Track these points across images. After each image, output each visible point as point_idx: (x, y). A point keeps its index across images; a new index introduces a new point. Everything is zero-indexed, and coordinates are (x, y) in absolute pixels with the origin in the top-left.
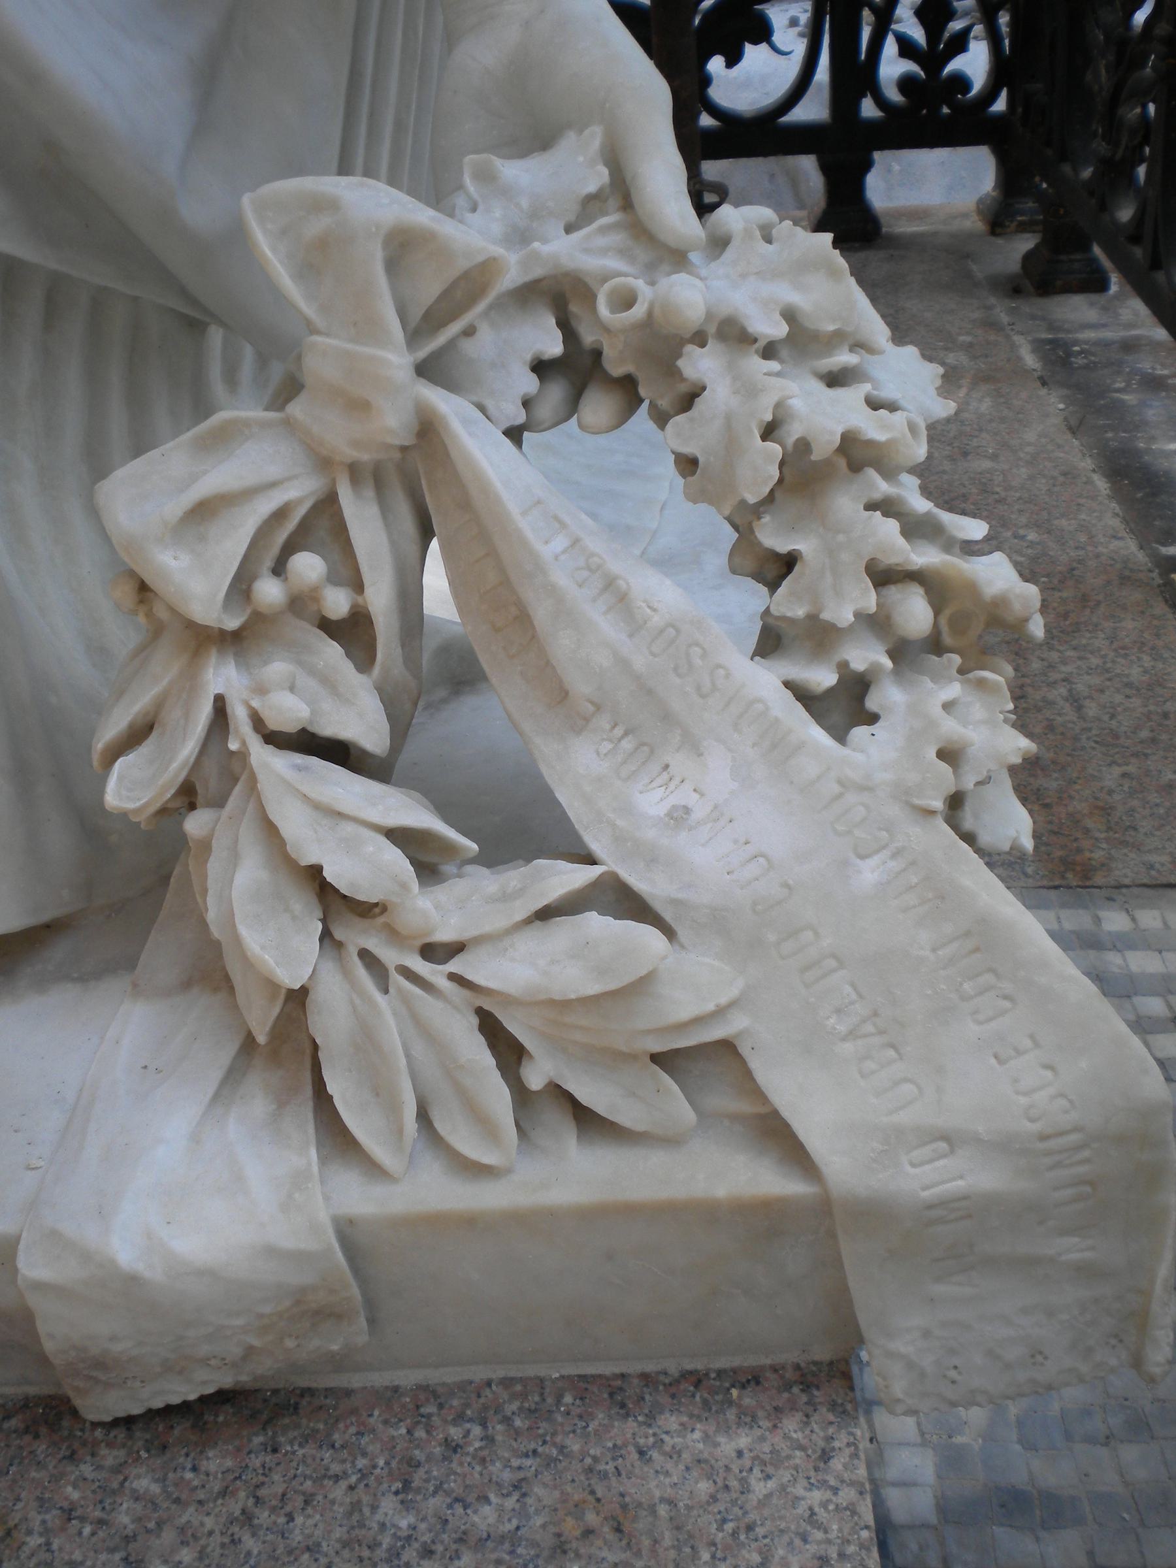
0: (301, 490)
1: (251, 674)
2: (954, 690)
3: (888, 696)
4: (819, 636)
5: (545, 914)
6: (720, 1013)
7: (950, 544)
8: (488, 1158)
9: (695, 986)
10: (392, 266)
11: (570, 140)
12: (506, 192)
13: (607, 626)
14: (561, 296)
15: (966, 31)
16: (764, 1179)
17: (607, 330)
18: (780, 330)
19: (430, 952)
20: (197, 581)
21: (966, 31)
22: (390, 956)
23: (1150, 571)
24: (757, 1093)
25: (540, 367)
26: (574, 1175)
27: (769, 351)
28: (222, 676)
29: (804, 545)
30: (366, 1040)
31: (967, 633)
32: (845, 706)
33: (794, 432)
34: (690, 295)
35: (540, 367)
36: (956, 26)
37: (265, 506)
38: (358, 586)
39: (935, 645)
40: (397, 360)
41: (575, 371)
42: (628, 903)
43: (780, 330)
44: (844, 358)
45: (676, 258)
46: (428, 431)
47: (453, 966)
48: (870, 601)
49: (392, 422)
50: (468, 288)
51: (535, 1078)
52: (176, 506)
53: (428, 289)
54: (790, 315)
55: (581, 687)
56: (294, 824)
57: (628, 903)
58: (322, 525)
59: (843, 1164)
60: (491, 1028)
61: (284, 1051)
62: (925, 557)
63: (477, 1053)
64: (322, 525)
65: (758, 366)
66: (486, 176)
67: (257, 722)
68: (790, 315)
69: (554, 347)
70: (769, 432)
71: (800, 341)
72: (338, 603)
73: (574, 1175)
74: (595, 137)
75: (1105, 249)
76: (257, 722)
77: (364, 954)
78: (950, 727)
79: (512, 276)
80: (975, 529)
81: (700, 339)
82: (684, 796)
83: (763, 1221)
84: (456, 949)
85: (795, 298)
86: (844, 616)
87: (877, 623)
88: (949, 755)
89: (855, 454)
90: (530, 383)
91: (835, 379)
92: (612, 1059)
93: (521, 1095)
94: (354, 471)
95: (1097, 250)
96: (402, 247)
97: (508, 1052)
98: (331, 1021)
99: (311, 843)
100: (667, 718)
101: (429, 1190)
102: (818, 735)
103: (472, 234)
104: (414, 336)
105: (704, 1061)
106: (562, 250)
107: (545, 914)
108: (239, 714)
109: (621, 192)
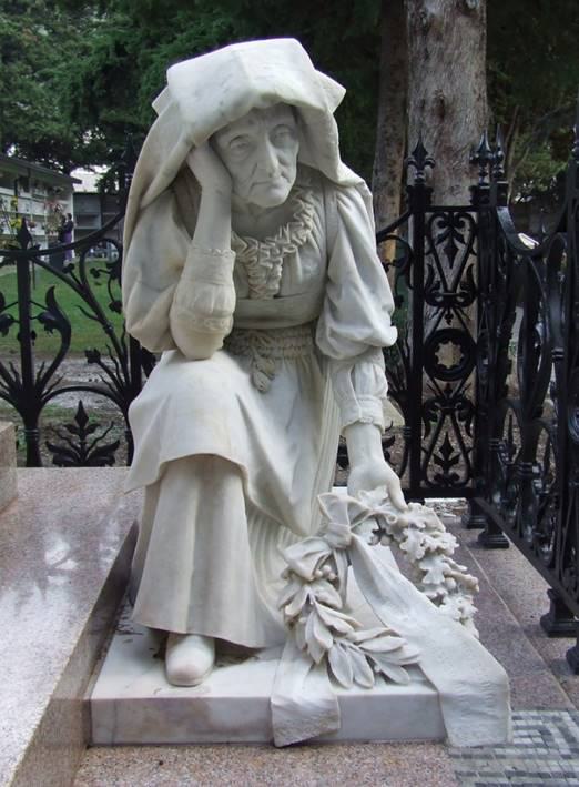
0: (327, 553)
1: (201, 677)
2: (460, 599)
3: (446, 599)
4: (432, 586)
5: (378, 636)
6: (415, 657)
7: (459, 571)
8: (368, 685)
9: (410, 650)
10: (349, 509)
11: (379, 488)
12: (367, 497)
13: (390, 582)
14: (378, 518)
15: (458, 456)
16: (426, 691)
17: (387, 524)
18: (424, 526)
19: (355, 643)
20: (307, 568)
21: (458, 456)
22: (346, 643)
23: (567, 757)
24: (423, 675)
25: (374, 532)
26: (383, 689)
27: (421, 530)
28: (308, 590)
29: (430, 569)
30: (342, 661)
31: (465, 587)
32: (438, 601)
33: (427, 546)
34: (407, 518)
35: (374, 532)
36: (453, 455)
37: (320, 555)
38: (337, 573)
39: (456, 591)
40: (349, 527)
41: (379, 533)
42: (394, 634)
43: (424, 526)
44: (436, 532)
45: (401, 511)
46: (353, 542)
47: (361, 646)
48: (444, 580)
49: (348, 539)
50: (362, 515)
51: (377, 669)
52: (303, 554)
53: (355, 514)
54: (425, 523)
55: (384, 593)
56: (324, 616)
57: (394, 634)
58: (331, 559)
59: (443, 688)
60: (368, 659)
61: (323, 664)
62: (454, 572)
63: (365, 663)
64: (331, 559)
65: (418, 532)
66: (363, 494)
67: (317, 599)
68: (425, 523)
69: (377, 528)
70: (422, 545)
71: (428, 528)
72: (333, 576)
73: (383, 689)
74: (385, 487)
75: (507, 534)
76: (317, 599)
77: (342, 645)
78: (460, 605)
79: (370, 514)
80: (465, 568)
81: (407, 527)
82: (407, 616)
83: (428, 698)
84: (361, 642)
85: (428, 521)
86: (438, 582)
87: (444, 585)
88: (461, 610)
89: (439, 551)
90: (372, 535)
91: (434, 537)
92: (392, 666)
93: (375, 673)
94: (337, 550)
95: (504, 534)
96: (351, 506)
97: (372, 664)
98: (334, 658)
99: (330, 621)
100: (402, 601)
101: (355, 691)
102: (435, 607)
103: (364, 504)
104: (351, 523)
105: (412, 667)
106: (380, 509)
107: (378, 636)
108: (312, 597)
109: (391, 498)
